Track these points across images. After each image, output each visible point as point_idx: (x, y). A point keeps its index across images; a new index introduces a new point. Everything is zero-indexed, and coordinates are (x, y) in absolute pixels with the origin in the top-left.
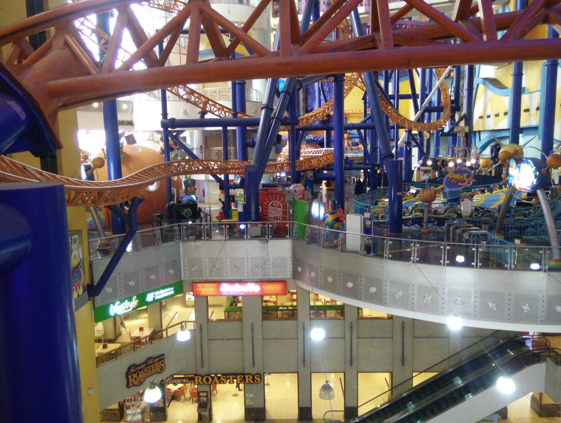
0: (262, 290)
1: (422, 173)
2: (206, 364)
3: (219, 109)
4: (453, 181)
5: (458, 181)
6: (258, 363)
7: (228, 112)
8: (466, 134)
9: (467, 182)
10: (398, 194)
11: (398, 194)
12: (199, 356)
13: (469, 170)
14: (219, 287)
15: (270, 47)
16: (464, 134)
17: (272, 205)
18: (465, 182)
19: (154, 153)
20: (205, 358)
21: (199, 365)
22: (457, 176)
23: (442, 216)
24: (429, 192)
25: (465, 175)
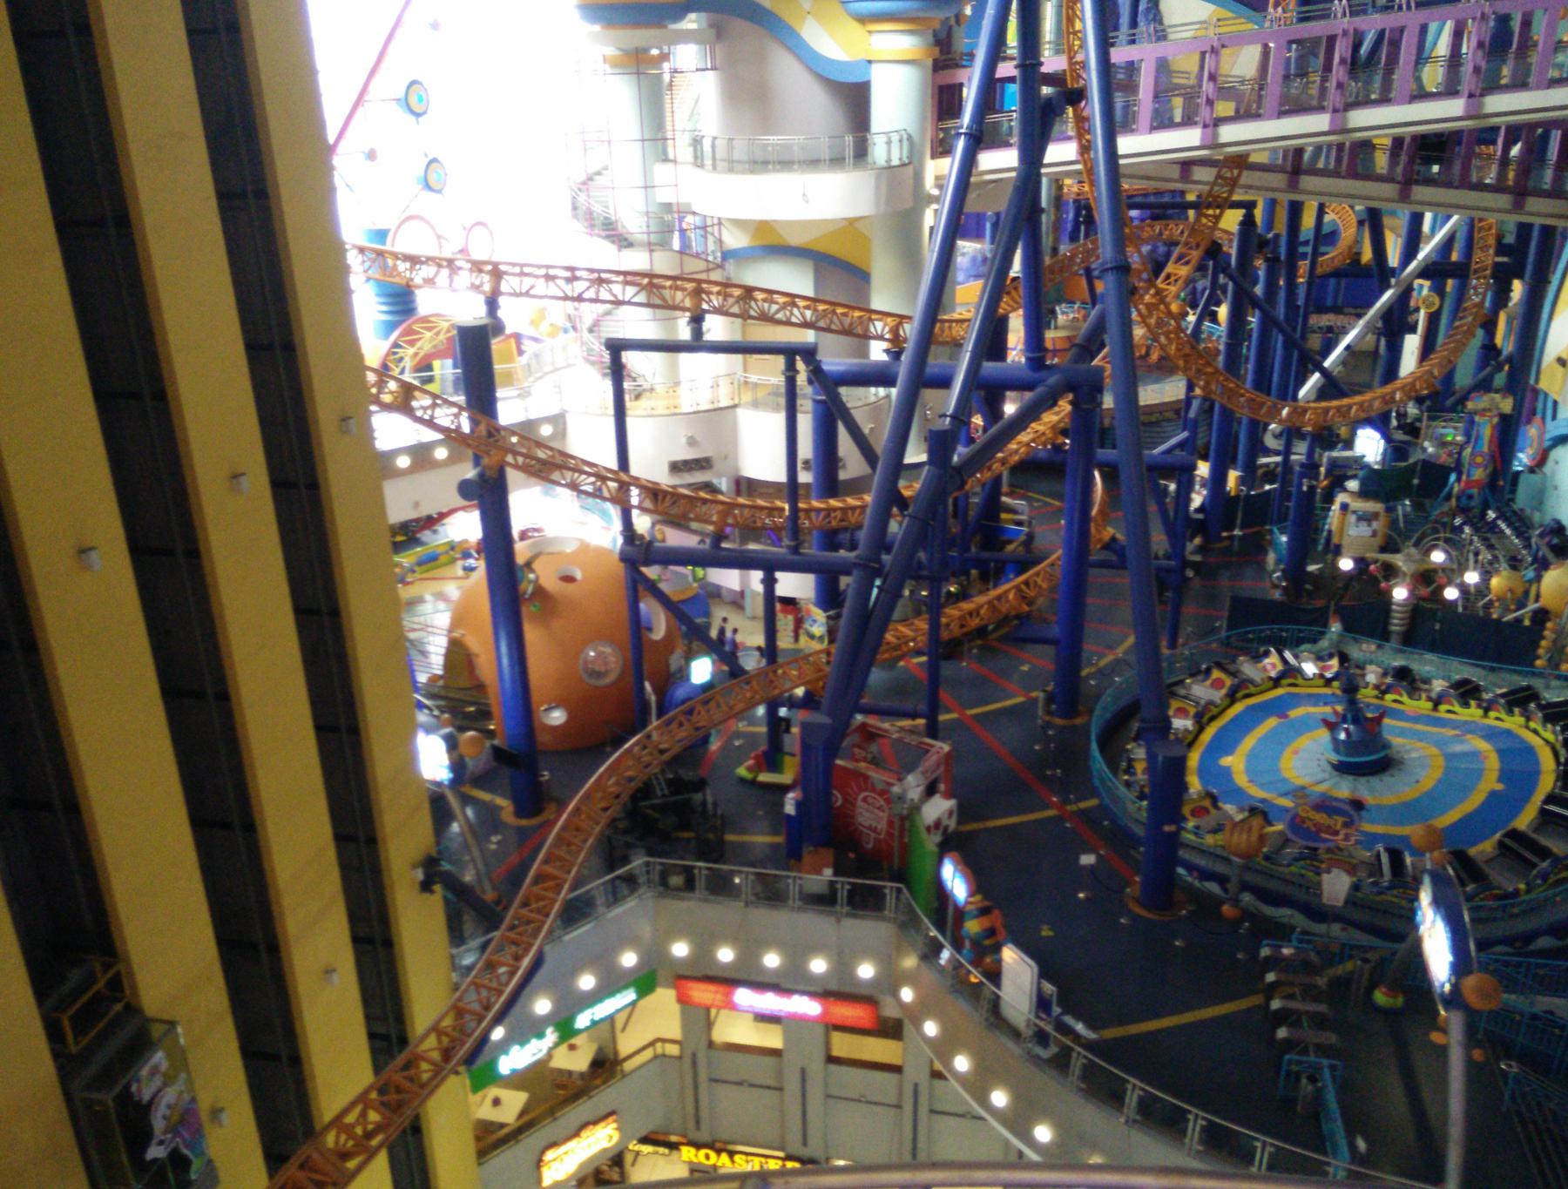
0: (825, 1013)
1: (1353, 518)
2: (705, 1125)
3: (783, 307)
4: (1308, 824)
5: (1320, 828)
6: (815, 1140)
7: (807, 307)
8: (1504, 417)
9: (1341, 836)
10: (1167, 828)
11: (1167, 828)
12: (690, 1109)
13: (1348, 808)
14: (729, 995)
15: (821, 726)
16: (1496, 420)
17: (865, 800)
18: (1336, 833)
19: (600, 552)
20: (704, 1113)
21: (691, 1124)
22: (1320, 818)
23: (1286, 870)
24: (1245, 837)
25: (1340, 820)
